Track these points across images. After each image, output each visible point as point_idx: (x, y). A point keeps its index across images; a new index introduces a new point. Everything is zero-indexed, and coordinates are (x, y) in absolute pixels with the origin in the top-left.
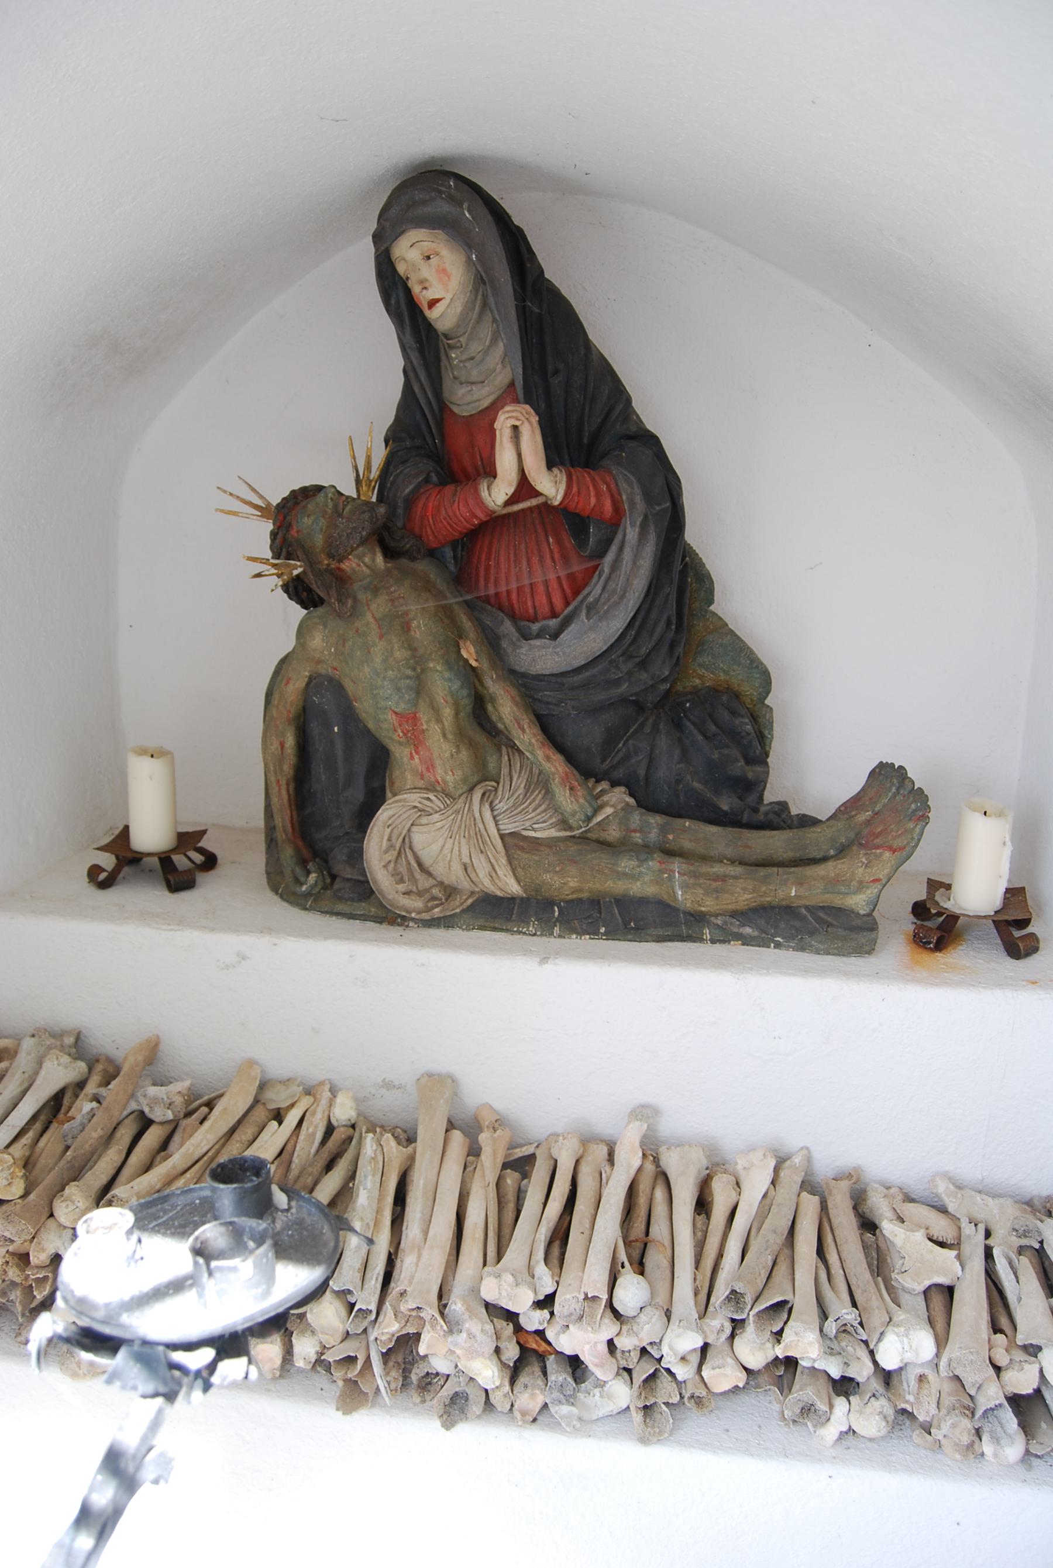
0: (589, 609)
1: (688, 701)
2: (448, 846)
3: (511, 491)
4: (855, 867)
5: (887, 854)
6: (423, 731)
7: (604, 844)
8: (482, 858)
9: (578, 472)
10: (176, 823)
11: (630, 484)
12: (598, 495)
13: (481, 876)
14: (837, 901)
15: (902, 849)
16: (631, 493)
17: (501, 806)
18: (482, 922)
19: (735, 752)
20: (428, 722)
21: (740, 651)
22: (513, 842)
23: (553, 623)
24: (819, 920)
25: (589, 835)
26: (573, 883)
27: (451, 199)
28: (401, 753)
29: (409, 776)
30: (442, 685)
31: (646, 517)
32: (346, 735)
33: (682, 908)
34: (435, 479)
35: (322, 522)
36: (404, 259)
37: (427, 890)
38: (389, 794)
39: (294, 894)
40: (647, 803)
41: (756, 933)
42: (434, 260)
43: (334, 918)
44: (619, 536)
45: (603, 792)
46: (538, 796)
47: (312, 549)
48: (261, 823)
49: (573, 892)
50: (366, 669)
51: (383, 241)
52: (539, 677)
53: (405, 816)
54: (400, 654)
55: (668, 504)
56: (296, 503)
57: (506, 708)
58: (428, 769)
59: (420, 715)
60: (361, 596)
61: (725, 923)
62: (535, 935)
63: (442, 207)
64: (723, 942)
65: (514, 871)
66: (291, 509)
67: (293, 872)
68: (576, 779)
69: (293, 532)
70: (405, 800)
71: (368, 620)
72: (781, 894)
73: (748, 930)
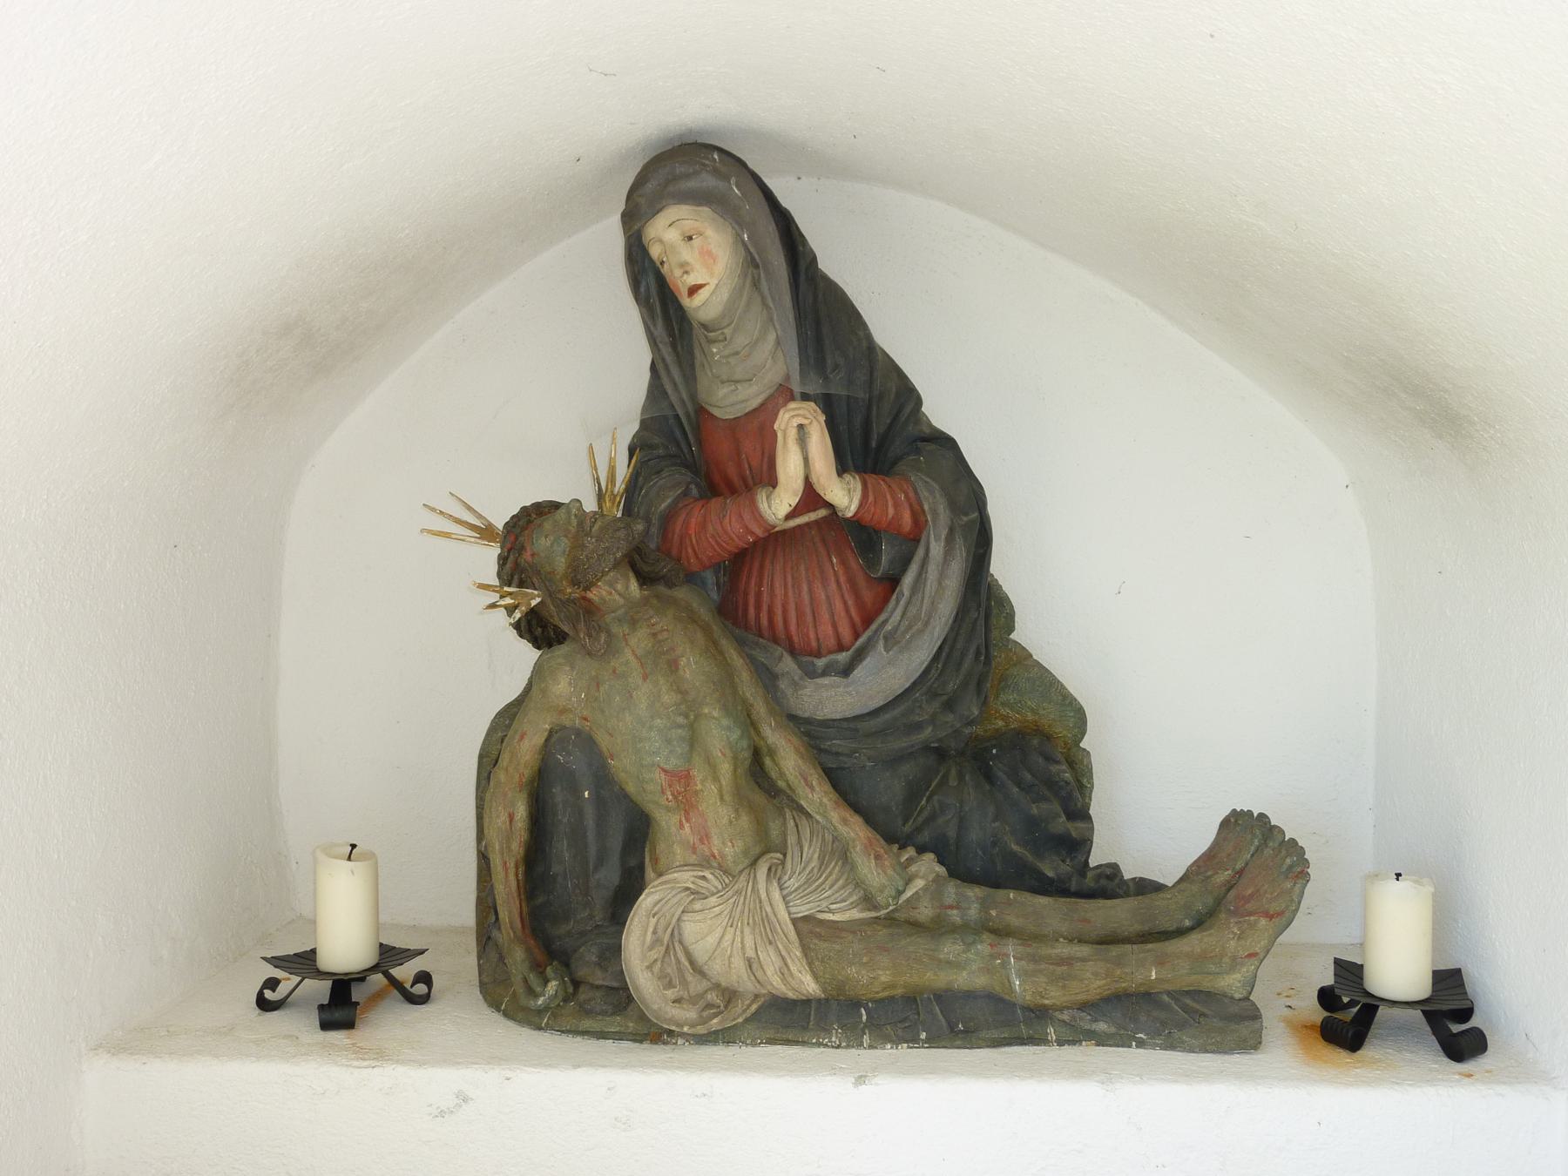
0: (886, 638)
1: (994, 746)
2: (728, 937)
3: (794, 501)
4: (1222, 938)
5: (1263, 922)
6: (696, 792)
7: (915, 926)
8: (771, 950)
9: (871, 479)
10: (378, 927)
11: (932, 492)
12: (896, 505)
13: (769, 973)
14: (1207, 984)
15: (1280, 914)
16: (936, 505)
17: (792, 883)
18: (770, 1034)
19: (1056, 807)
20: (703, 781)
21: (1048, 685)
22: (808, 928)
23: (843, 657)
24: (1185, 1009)
25: (897, 915)
26: (885, 977)
27: (716, 172)
28: (667, 822)
29: (678, 849)
30: (720, 735)
31: (951, 530)
32: (599, 801)
33: (1020, 1001)
34: (695, 491)
35: (565, 543)
36: (661, 241)
37: (701, 996)
38: (649, 873)
39: (526, 1009)
40: (960, 871)
41: (1113, 1030)
42: (696, 242)
43: (579, 1039)
44: (920, 552)
45: (910, 861)
46: (835, 868)
47: (547, 576)
48: (467, 915)
49: (884, 989)
50: (628, 718)
51: (634, 218)
52: (827, 723)
53: (675, 900)
54: (668, 698)
55: (976, 514)
56: (530, 522)
57: (790, 762)
58: (701, 840)
59: (694, 772)
60: (615, 629)
61: (1074, 1018)
62: (839, 1047)
63: (708, 181)
64: (1073, 1042)
65: (810, 964)
66: (524, 529)
67: (526, 981)
68: (880, 845)
69: (527, 556)
70: (675, 881)
71: (627, 658)
72: (1139, 978)
73: (1102, 1026)
